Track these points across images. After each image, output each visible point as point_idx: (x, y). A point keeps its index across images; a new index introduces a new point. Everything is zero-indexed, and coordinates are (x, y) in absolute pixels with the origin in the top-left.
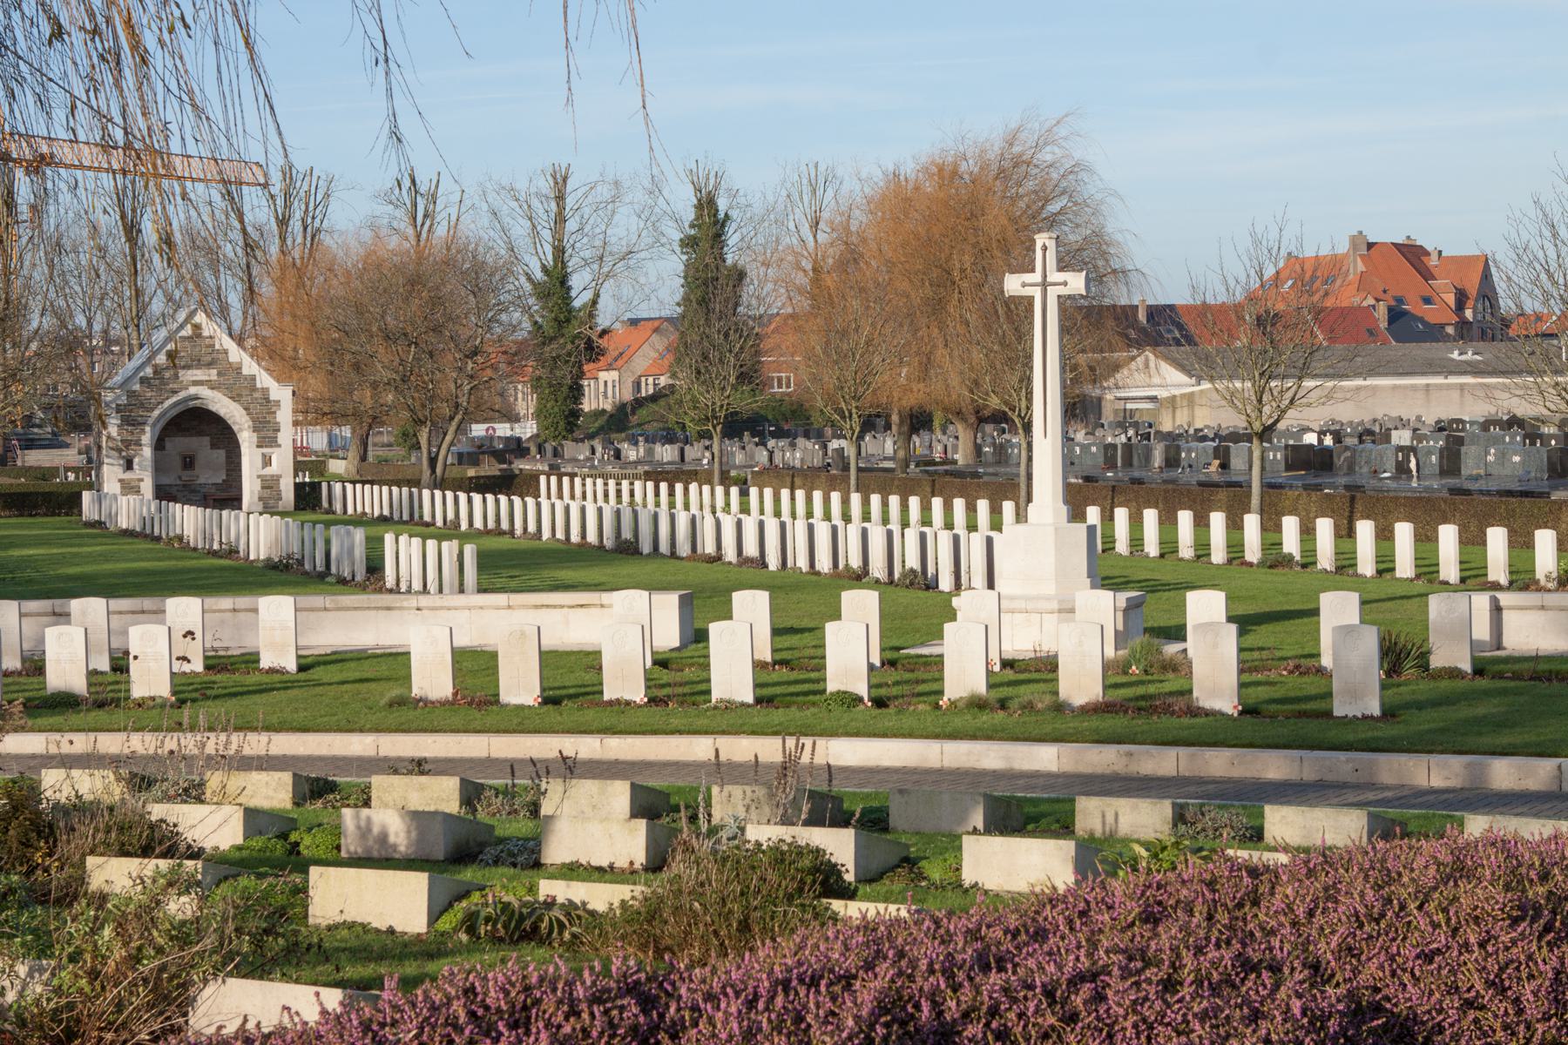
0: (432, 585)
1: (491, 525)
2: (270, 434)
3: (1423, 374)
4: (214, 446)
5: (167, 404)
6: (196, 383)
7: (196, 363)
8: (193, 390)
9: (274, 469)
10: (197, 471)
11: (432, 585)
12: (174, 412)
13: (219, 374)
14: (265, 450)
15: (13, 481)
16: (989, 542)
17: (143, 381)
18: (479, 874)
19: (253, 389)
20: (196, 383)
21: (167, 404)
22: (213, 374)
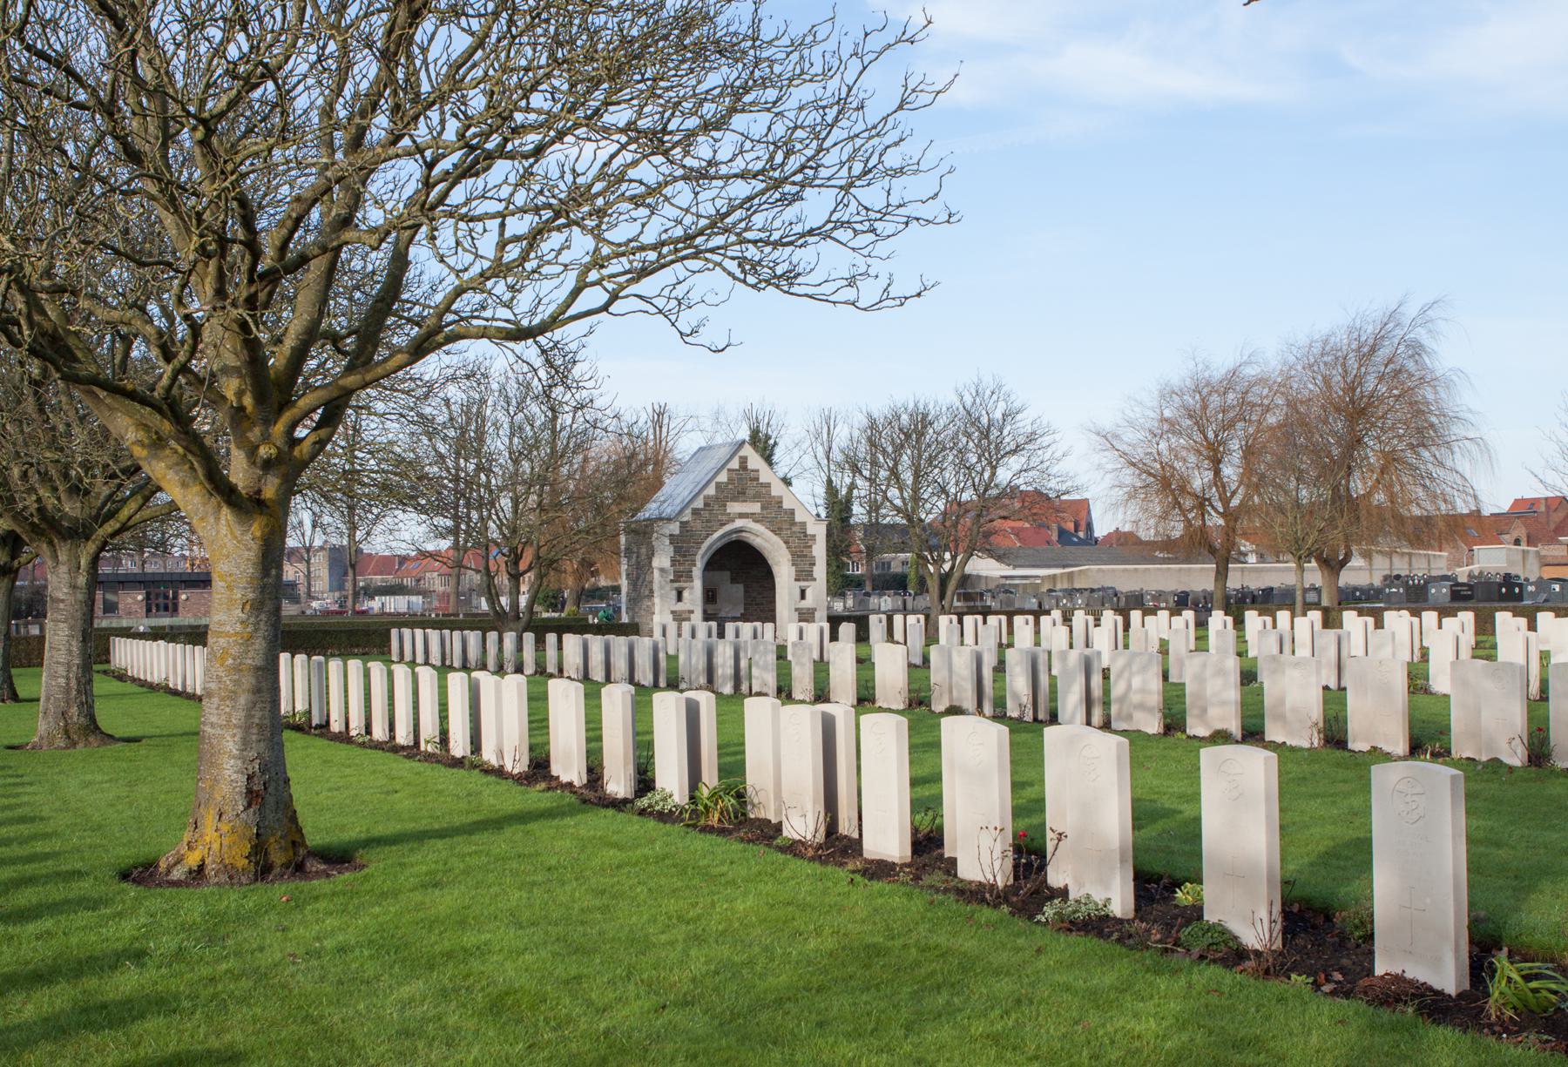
0: (491, 662)
1: (551, 638)
2: (807, 568)
3: (1049, 566)
4: (734, 580)
5: (716, 535)
6: (742, 516)
7: (740, 495)
8: (739, 523)
9: (808, 603)
10: (718, 605)
11: (491, 662)
12: (719, 545)
13: (763, 508)
14: (803, 584)
15: (556, 615)
16: (1037, 644)
17: (696, 512)
18: (62, 657)
19: (793, 523)
20: (742, 516)
21: (716, 535)
22: (756, 508)
